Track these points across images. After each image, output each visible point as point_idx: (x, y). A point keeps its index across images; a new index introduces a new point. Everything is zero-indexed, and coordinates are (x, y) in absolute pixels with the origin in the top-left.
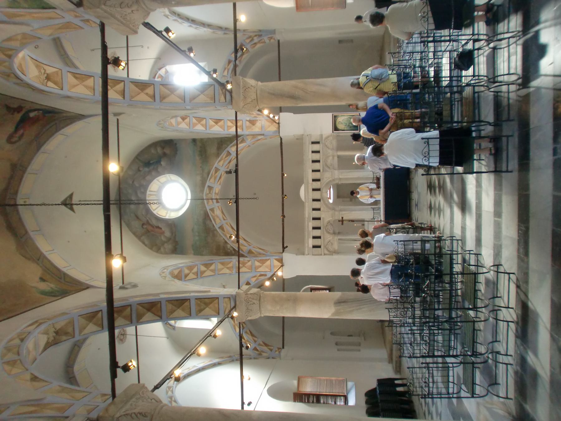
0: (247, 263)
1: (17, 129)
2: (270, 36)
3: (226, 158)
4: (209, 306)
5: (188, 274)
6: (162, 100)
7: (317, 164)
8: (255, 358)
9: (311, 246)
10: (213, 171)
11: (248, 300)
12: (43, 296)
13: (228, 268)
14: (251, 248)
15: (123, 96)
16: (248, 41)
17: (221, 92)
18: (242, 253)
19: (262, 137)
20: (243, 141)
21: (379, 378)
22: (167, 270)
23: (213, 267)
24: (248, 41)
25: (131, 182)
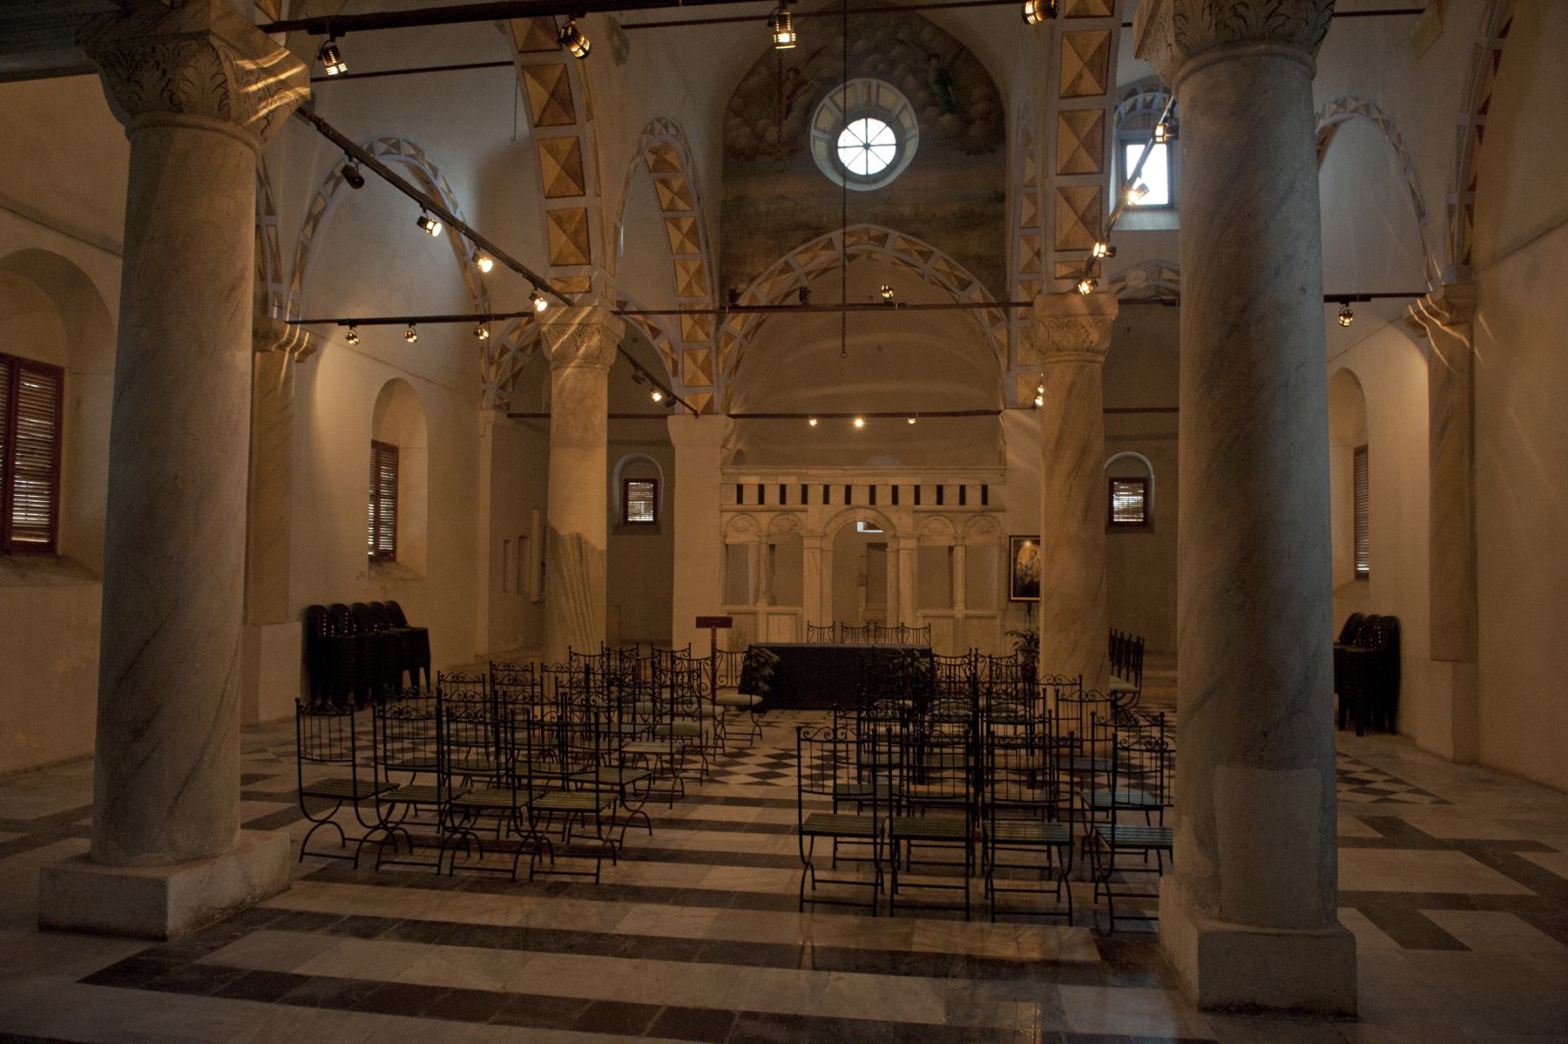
0: (703, 328)
3: (954, 279)
4: (570, 242)
5: (670, 189)
9: (743, 480)
10: (924, 246)
13: (689, 284)
15: (1072, 14)
18: (727, 320)
19: (1004, 368)
20: (994, 319)
23: (690, 247)
25: (900, 36)
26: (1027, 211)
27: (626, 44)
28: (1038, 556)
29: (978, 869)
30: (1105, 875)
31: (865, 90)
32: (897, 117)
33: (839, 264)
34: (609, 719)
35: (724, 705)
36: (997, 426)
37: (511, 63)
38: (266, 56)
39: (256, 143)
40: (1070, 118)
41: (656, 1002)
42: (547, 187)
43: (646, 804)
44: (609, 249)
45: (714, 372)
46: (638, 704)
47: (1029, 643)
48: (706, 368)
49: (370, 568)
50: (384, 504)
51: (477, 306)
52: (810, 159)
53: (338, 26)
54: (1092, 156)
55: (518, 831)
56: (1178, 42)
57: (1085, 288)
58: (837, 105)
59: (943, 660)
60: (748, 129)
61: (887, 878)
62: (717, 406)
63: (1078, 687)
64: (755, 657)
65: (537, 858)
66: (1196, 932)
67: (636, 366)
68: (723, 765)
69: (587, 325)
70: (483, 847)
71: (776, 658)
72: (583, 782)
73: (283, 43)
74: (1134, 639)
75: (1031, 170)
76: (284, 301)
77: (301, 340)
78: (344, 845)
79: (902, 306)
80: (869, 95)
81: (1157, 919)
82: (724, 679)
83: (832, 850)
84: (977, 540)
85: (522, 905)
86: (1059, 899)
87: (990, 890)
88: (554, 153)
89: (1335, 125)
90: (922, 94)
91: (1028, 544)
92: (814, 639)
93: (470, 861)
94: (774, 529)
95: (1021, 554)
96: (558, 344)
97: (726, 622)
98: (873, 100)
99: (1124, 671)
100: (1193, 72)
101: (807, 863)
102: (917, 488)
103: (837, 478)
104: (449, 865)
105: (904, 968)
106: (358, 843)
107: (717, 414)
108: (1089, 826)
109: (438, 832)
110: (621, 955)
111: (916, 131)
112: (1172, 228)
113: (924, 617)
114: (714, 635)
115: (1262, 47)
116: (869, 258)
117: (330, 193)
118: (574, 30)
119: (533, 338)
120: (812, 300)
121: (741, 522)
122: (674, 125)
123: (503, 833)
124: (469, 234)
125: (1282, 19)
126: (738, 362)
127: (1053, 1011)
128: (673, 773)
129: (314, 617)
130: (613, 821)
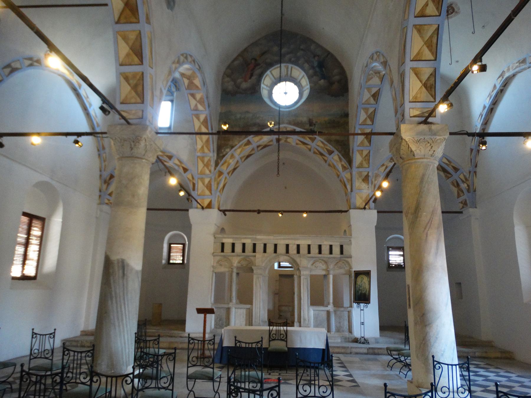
0: (208, 168)
2: (468, 202)
3: (325, 150)
4: (133, 91)
6: (416, 28)
7: (317, 251)
8: (101, 176)
9: (224, 241)
11: (137, 141)
13: (202, 147)
14: (225, 174)
16: (462, 176)
17: (425, 110)
19: (349, 190)
24: (462, 176)
25: (302, 47)
31: (285, 70)
40: (419, 29)
42: (121, 60)
48: (209, 187)
80: (287, 71)
89: (514, 75)
98: (289, 73)
111: (308, 86)
114: (205, 318)
122: (198, 63)
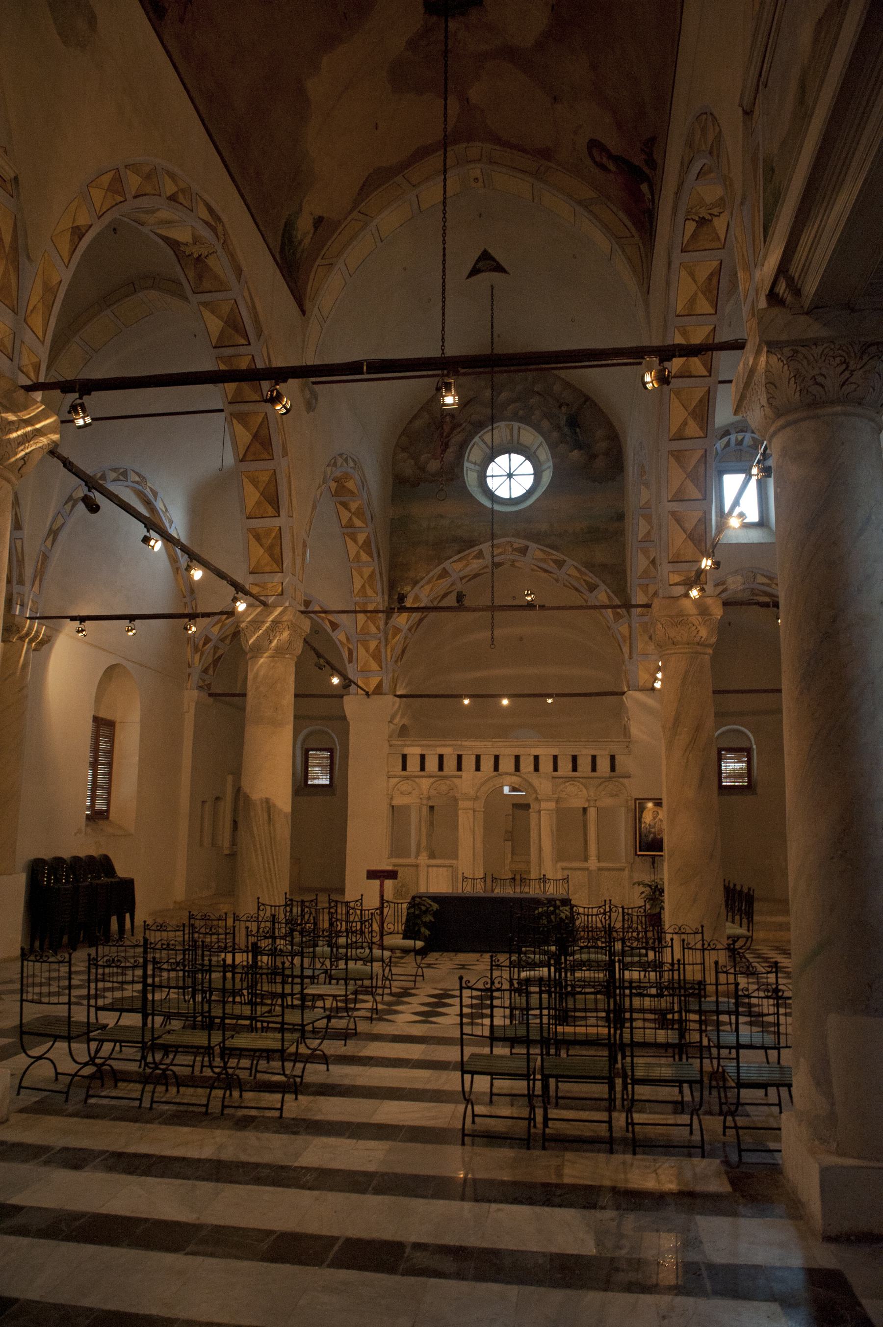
0: (374, 624)
1: (615, 159)
3: (583, 583)
4: (266, 555)
5: (349, 510)
6: (673, 455)
9: (407, 751)
12: (283, 222)
13: (363, 586)
15: (678, 374)
19: (627, 656)
20: (618, 617)
21: (136, 883)
22: (354, 468)
23: (364, 557)
26: (643, 527)
27: (315, 396)
28: (660, 816)
29: (618, 1102)
30: (729, 1109)
32: (535, 453)
33: (489, 570)
34: (292, 963)
35: (392, 950)
36: (622, 703)
37: (222, 411)
38: (25, 409)
39: (13, 479)
40: (678, 456)
41: (335, 1233)
42: (248, 510)
43: (325, 1042)
44: (299, 560)
45: (383, 659)
46: (317, 949)
47: (654, 893)
48: (377, 656)
49: (87, 825)
50: (101, 770)
51: (186, 604)
52: (464, 488)
53: (87, 387)
54: (696, 486)
55: (211, 1067)
56: (770, 404)
57: (694, 593)
58: (485, 443)
59: (581, 910)
60: (413, 462)
61: (539, 1112)
62: (386, 687)
63: (700, 935)
64: (417, 903)
65: (228, 1092)
66: (817, 1166)
67: (319, 656)
68: (390, 1004)
69: (279, 622)
70: (181, 1082)
71: (435, 907)
72: (268, 1022)
73: (39, 399)
74: (745, 890)
75: (645, 495)
76: (26, 600)
77: (38, 632)
78: (57, 1079)
79: (542, 607)
80: (512, 435)
81: (780, 1151)
82: (390, 926)
83: (489, 1085)
84: (607, 802)
85: (214, 1138)
86: (691, 1133)
87: (630, 1124)
88: (255, 482)
90: (555, 435)
91: (650, 805)
92: (467, 890)
93: (168, 1095)
94: (433, 792)
95: (645, 814)
96: (254, 638)
97: (392, 875)
99: (737, 918)
100: (783, 427)
101: (467, 1098)
102: (555, 758)
103: (487, 748)
104: (149, 1099)
105: (557, 1200)
106: (70, 1078)
107: (385, 694)
108: (715, 1062)
109: (140, 1067)
110: (303, 1187)
111: (550, 464)
112: (763, 541)
113: (563, 869)
114: (382, 886)
115: (838, 409)
116: (513, 565)
117: (68, 511)
118: (278, 393)
119: (232, 630)
120: (467, 602)
121: (405, 786)
123: (197, 1069)
124: (184, 549)
125: (854, 386)
126: (403, 651)
127: (690, 1242)
128: (348, 1012)
129: (36, 868)
130: (297, 1058)
